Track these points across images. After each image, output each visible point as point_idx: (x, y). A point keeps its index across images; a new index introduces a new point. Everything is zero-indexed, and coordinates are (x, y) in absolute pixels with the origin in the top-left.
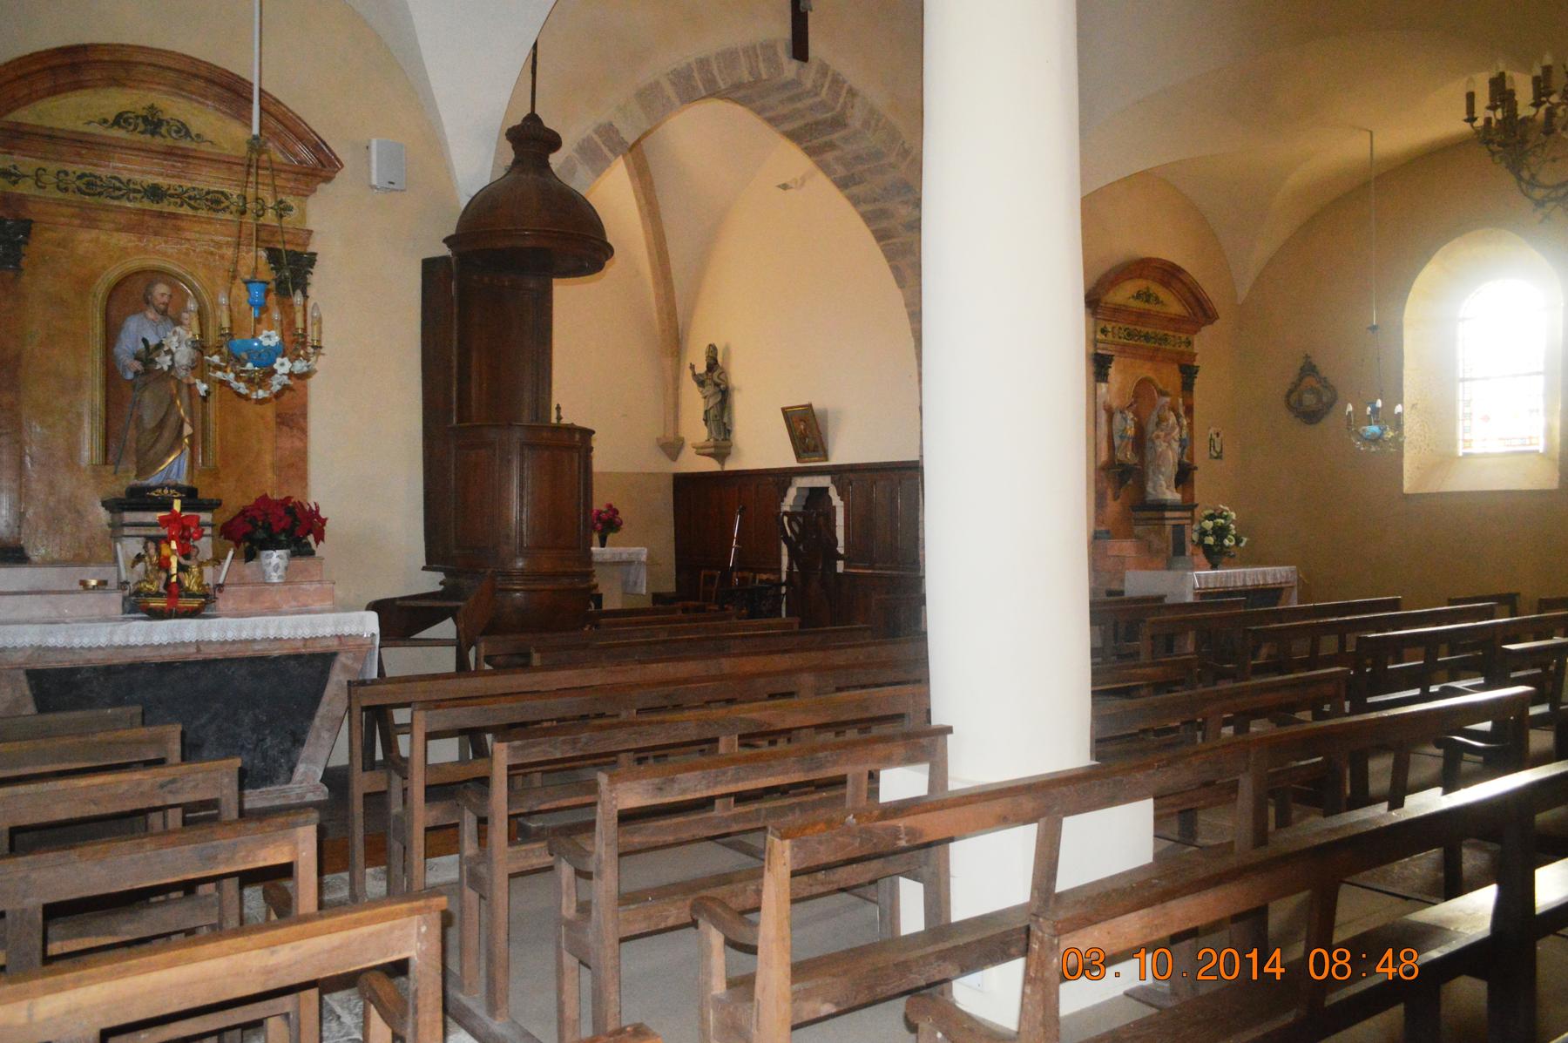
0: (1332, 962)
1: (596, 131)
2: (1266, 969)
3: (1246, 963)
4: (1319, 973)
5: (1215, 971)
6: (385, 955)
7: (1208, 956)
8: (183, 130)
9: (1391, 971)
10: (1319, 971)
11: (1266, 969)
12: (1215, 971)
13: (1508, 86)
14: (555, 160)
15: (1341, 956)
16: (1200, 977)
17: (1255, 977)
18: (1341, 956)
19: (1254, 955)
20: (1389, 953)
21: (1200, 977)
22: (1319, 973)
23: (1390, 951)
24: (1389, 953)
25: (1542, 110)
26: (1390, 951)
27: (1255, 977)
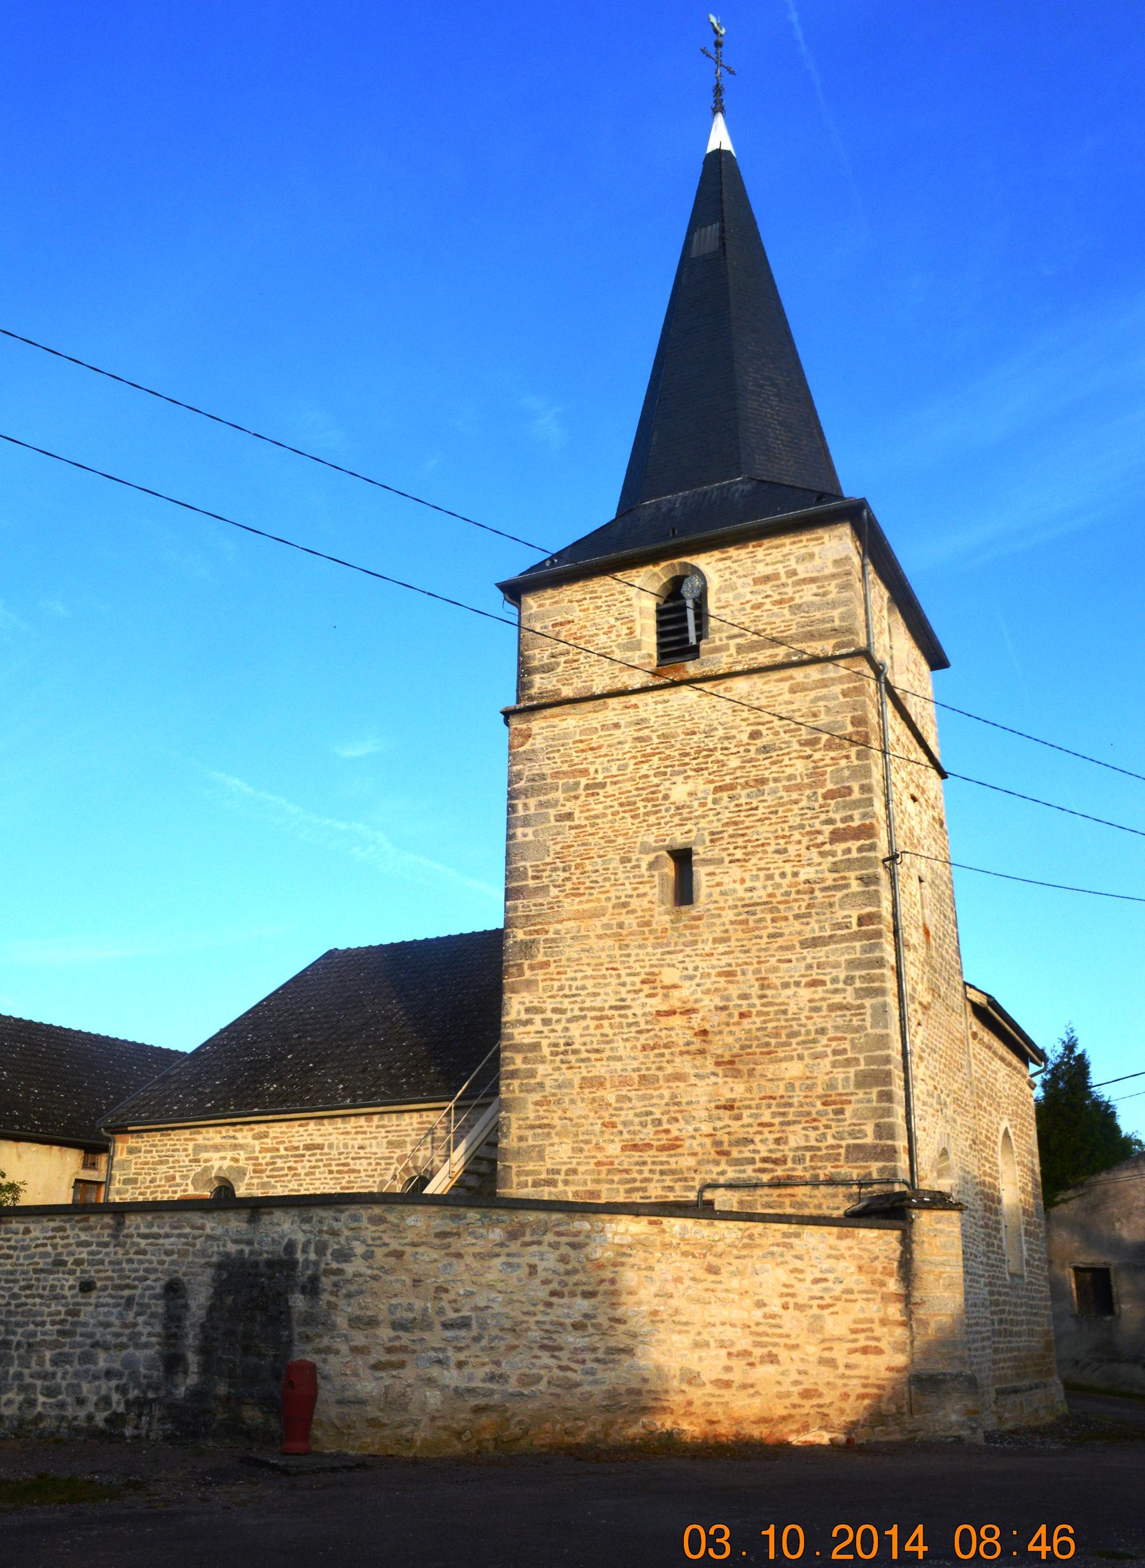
0: (979, 1540)
1: (290, 1240)
2: (908, 1547)
3: (885, 1542)
4: (965, 1551)
5: (851, 1549)
6: (671, 564)
7: (843, 1535)
8: (455, 1148)
9: (1044, 1549)
10: (965, 1549)
11: (908, 1547)
12: (851, 1549)
13: (303, 1353)
14: (717, 1207)
15: (990, 1533)
16: (835, 1556)
17: (895, 1556)
18: (990, 1533)
19: (894, 1532)
20: (1043, 1530)
21: (835, 1556)
22: (965, 1551)
23: (1044, 1527)
24: (1043, 1530)
25: (31, 1380)
26: (1044, 1527)
27: (895, 1556)
